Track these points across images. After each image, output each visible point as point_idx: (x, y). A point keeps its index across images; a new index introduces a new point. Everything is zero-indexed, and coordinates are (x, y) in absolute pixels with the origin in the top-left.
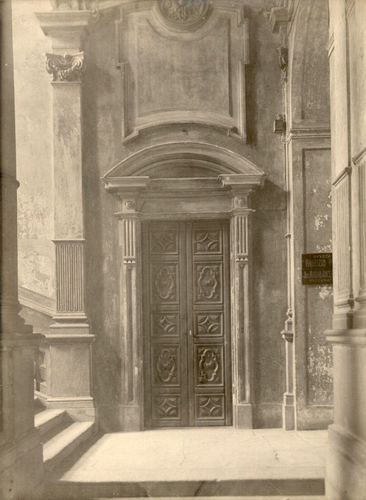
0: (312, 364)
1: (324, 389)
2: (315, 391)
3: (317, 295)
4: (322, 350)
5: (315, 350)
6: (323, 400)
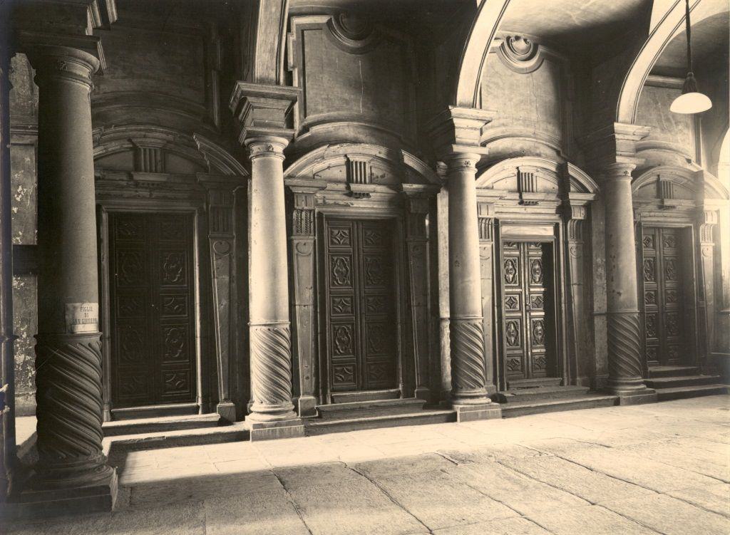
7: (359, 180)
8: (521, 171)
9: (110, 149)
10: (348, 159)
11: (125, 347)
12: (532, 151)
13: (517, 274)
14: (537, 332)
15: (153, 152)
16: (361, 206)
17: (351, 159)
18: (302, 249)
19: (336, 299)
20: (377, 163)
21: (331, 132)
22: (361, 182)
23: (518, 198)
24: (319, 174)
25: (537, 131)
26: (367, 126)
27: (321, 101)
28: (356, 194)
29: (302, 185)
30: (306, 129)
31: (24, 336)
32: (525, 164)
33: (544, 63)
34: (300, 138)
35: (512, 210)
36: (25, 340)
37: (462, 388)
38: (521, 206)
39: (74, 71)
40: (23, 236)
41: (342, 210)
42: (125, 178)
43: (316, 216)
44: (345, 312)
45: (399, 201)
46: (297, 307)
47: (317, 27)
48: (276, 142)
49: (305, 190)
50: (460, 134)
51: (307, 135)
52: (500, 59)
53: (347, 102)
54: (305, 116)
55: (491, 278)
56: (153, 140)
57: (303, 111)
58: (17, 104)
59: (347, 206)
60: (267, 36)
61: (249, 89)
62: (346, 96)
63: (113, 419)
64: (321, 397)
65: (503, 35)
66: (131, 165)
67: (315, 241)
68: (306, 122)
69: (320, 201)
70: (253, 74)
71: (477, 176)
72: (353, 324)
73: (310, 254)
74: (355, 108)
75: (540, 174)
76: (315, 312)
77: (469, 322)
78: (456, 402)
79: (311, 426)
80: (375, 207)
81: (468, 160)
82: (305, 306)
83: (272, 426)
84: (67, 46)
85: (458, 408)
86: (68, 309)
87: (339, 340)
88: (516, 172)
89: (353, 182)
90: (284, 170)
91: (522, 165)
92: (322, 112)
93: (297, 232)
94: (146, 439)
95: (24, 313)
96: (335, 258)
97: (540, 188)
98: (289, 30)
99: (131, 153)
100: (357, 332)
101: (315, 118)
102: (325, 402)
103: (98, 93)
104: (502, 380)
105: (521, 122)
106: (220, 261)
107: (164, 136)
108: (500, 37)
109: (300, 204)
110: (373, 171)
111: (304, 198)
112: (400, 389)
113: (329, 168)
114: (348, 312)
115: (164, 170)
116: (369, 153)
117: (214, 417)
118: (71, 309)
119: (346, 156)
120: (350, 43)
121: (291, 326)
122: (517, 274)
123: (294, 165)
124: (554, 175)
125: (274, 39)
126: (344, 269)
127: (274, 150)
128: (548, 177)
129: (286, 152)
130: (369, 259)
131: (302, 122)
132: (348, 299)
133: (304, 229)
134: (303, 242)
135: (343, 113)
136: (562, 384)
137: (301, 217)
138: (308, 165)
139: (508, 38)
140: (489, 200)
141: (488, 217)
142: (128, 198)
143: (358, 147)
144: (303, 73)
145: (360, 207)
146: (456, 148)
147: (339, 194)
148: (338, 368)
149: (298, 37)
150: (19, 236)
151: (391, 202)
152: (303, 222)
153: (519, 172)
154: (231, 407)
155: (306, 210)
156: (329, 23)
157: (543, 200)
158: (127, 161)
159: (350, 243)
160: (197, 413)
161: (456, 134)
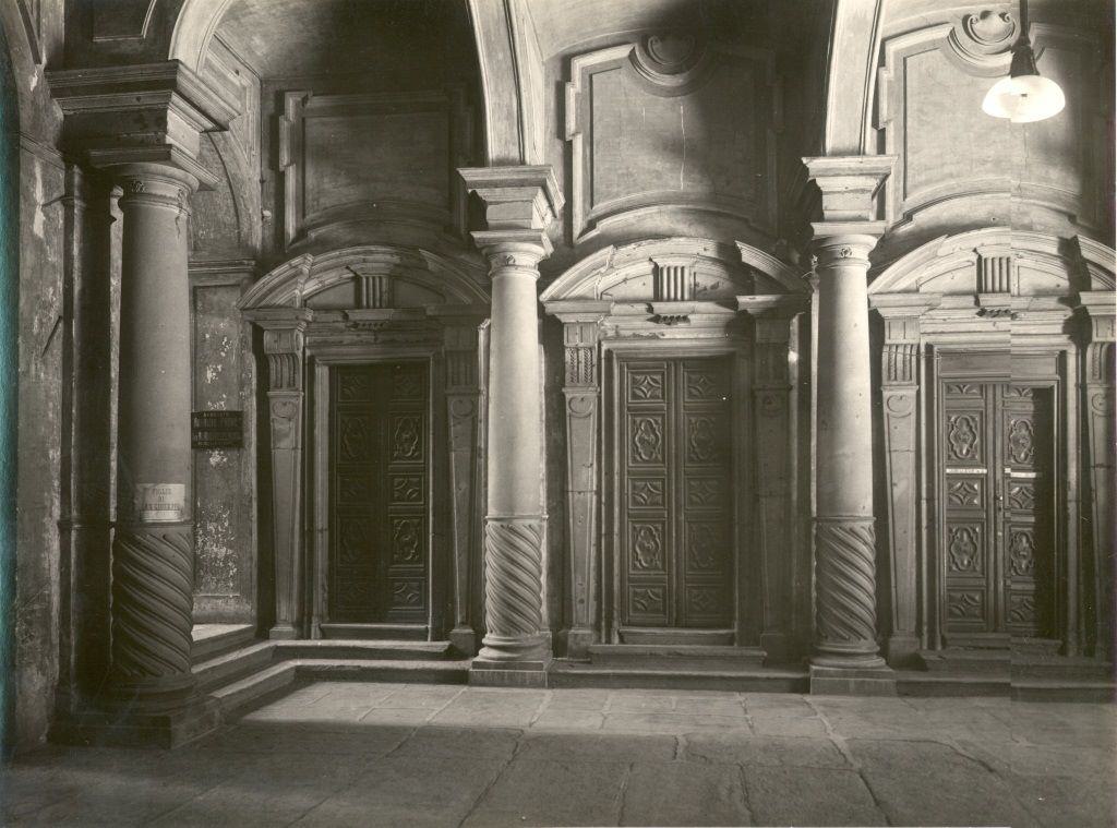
7: (997, 285)
8: (984, 256)
10: (656, 264)
15: (378, 280)
16: (678, 337)
17: (660, 265)
18: (577, 406)
19: (638, 483)
21: (633, 224)
22: (675, 299)
23: (972, 304)
24: (610, 292)
25: (1025, 183)
28: (665, 318)
30: (591, 225)
33: (1044, 54)
34: (582, 240)
35: (963, 327)
36: (227, 529)
37: (826, 637)
39: (154, 192)
40: (228, 400)
41: (645, 344)
42: (340, 319)
43: (603, 356)
44: (652, 504)
45: (739, 325)
46: (570, 494)
47: (615, 66)
49: (581, 318)
50: (831, 205)
51: (593, 233)
52: (948, 58)
54: (592, 205)
58: (223, 236)
59: (654, 337)
60: (500, 96)
63: (324, 636)
64: (604, 632)
65: (956, 15)
66: (350, 300)
67: (918, 393)
68: (593, 215)
69: (611, 333)
71: (872, 276)
72: (663, 523)
74: (672, 183)
76: (599, 502)
77: (841, 525)
79: (559, 674)
80: (701, 336)
82: (580, 493)
86: (137, 491)
87: (642, 547)
88: (974, 258)
90: (869, 283)
91: (982, 245)
92: (617, 195)
94: (338, 667)
95: (227, 495)
98: (882, 63)
101: (607, 207)
102: (609, 641)
104: (932, 631)
105: (989, 165)
106: (459, 427)
107: (388, 257)
108: (948, 20)
109: (894, 336)
111: (578, 331)
112: (736, 630)
113: (625, 280)
114: (657, 504)
115: (391, 304)
116: (691, 253)
117: (442, 645)
118: (141, 490)
120: (667, 81)
123: (557, 282)
124: (1058, 262)
125: (511, 99)
126: (652, 436)
127: (517, 263)
128: (1046, 267)
132: (659, 484)
134: (579, 395)
135: (652, 193)
136: (1063, 651)
137: (894, 357)
138: (579, 280)
139: (966, 19)
143: (668, 243)
144: (590, 142)
145: (679, 338)
146: (819, 229)
147: (640, 320)
148: (638, 590)
149: (583, 87)
150: (222, 399)
151: (729, 326)
152: (582, 366)
153: (980, 257)
154: (469, 634)
156: (632, 57)
157: (1027, 310)
159: (663, 395)
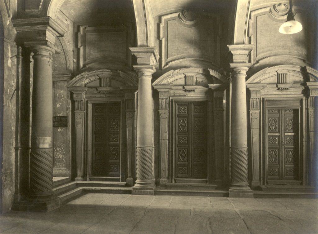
0: (55, 154)
1: (59, 163)
2: (56, 163)
3: (57, 130)
4: (58, 149)
5: (56, 149)
6: (59, 166)
9: (92, 80)
11: (196, 156)
12: (288, 62)
13: (277, 126)
14: (288, 156)
17: (187, 75)
20: (200, 76)
22: (191, 85)
24: (172, 83)
26: (195, 59)
27: (174, 51)
28: (188, 90)
29: (161, 88)
30: (167, 64)
31: (63, 148)
32: (280, 69)
34: (164, 68)
38: (278, 91)
39: (42, 54)
41: (182, 98)
43: (170, 101)
45: (209, 92)
47: (174, 19)
48: (146, 71)
49: (164, 90)
50: (235, 58)
51: (168, 66)
53: (186, 50)
54: (167, 58)
55: (258, 127)
56: (105, 75)
57: (166, 56)
59: (185, 96)
61: (134, 51)
62: (186, 47)
63: (91, 180)
66: (98, 85)
67: (260, 112)
70: (234, 42)
73: (166, 118)
75: (292, 73)
76: (169, 142)
78: (230, 188)
81: (240, 70)
82: (163, 140)
83: (139, 189)
84: (39, 45)
85: (232, 189)
89: (280, 83)
91: (279, 70)
93: (161, 108)
94: (94, 189)
96: (180, 119)
97: (291, 81)
98: (250, 18)
99: (99, 80)
100: (189, 153)
102: (172, 182)
103: (89, 59)
105: (280, 47)
107: (109, 73)
109: (253, 96)
110: (197, 79)
113: (177, 80)
114: (185, 143)
117: (124, 183)
119: (276, 71)
120: (189, 23)
121: (248, 149)
122: (277, 126)
126: (184, 124)
129: (247, 73)
130: (196, 119)
131: (166, 61)
133: (255, 106)
134: (163, 112)
136: (302, 184)
137: (253, 102)
139: (274, 6)
140: (257, 89)
141: (257, 97)
142: (98, 97)
144: (167, 40)
148: (180, 168)
149: (165, 24)
150: (62, 113)
151: (206, 93)
152: (164, 104)
154: (132, 180)
155: (165, 99)
157: (292, 87)
158: (97, 84)
159: (187, 112)
160: (120, 181)
161: (233, 58)
